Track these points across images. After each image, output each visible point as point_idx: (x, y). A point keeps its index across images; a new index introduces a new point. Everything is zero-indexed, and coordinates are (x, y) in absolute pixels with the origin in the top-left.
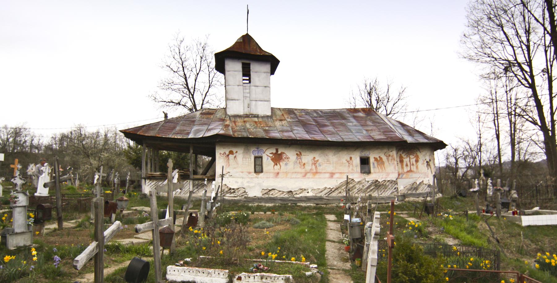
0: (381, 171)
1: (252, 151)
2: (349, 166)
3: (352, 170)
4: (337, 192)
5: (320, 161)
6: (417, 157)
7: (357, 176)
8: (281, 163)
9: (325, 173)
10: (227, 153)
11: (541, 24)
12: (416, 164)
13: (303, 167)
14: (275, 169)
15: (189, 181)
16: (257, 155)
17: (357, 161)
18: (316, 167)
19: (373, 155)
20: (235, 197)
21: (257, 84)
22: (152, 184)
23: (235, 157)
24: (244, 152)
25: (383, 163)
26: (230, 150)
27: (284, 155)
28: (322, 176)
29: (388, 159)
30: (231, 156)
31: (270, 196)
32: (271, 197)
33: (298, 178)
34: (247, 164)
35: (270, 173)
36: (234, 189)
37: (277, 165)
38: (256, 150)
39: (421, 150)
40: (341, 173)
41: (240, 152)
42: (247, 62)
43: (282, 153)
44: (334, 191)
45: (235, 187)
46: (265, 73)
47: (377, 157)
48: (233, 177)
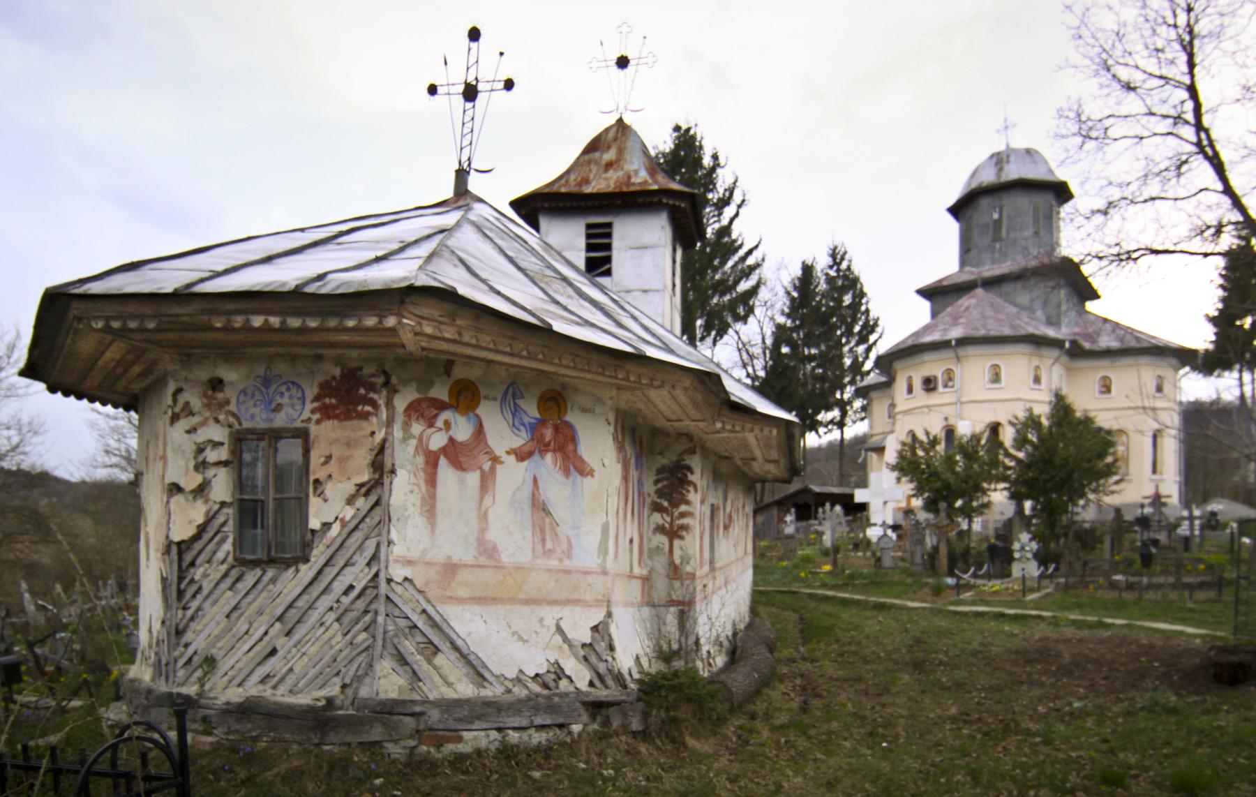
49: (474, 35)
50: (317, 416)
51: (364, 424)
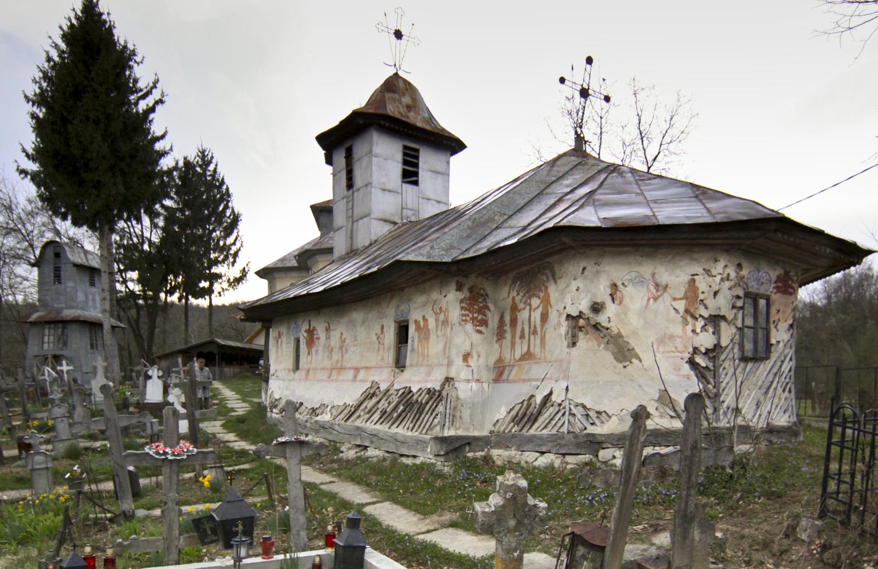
2: (379, 350)
5: (347, 341)
33: (324, 381)
49: (589, 61)
50: (775, 291)
51: (790, 297)
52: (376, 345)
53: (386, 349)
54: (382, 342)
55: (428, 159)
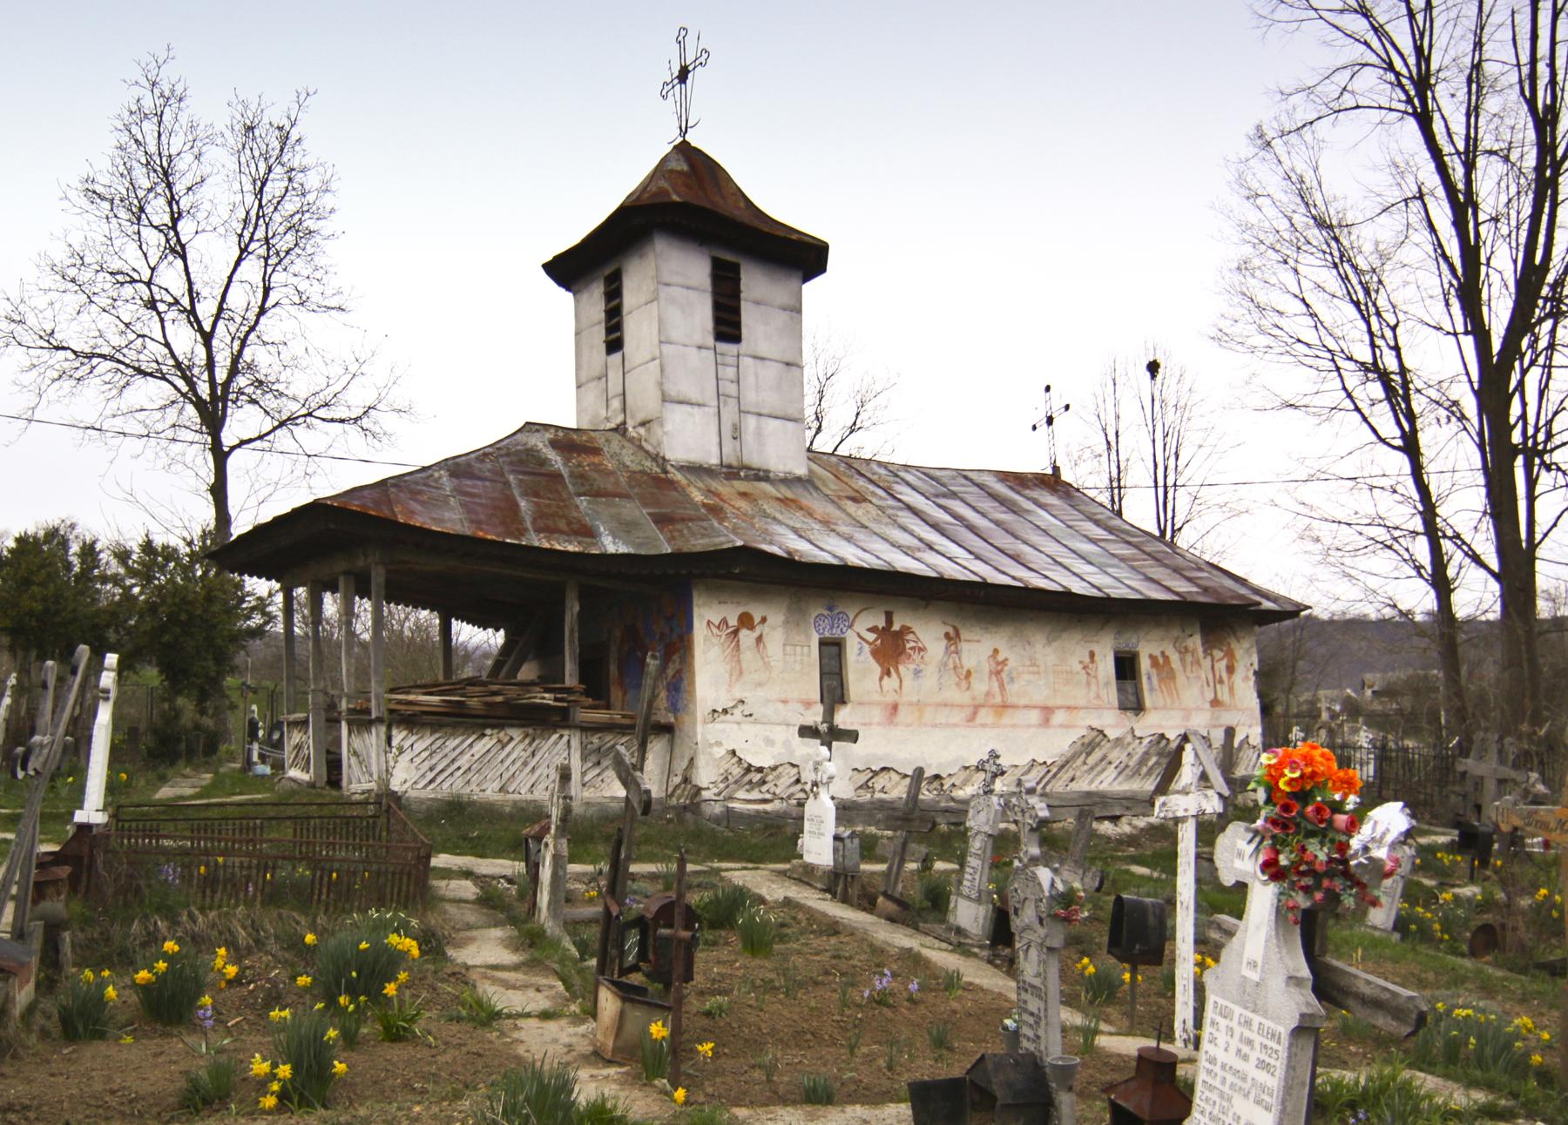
0: (1169, 702)
1: (814, 615)
2: (1088, 684)
3: (1098, 697)
4: (1065, 776)
5: (1012, 664)
6: (1230, 655)
7: (1113, 723)
8: (901, 668)
9: (1026, 707)
10: (733, 622)
11: (200, 330)
12: (1229, 678)
13: (964, 684)
14: (885, 688)
15: (566, 732)
16: (827, 634)
17: (1107, 667)
18: (1002, 686)
19: (1148, 648)
20: (765, 801)
21: (763, 350)
22: (419, 746)
23: (759, 639)
24: (787, 622)
25: (1171, 676)
26: (741, 610)
27: (910, 637)
28: (1020, 717)
29: (1183, 660)
30: (747, 637)
31: (878, 795)
32: (882, 801)
33: (955, 725)
34: (798, 667)
35: (870, 704)
36: (760, 770)
37: (888, 674)
38: (826, 613)
39: (1240, 634)
40: (1069, 708)
41: (773, 618)
42: (728, 257)
43: (906, 630)
44: (1055, 776)
45: (767, 763)
46: (784, 309)
47: (1157, 653)
48: (756, 722)
52: (1084, 677)
53: (1101, 684)
54: (1092, 673)
55: (755, 284)
